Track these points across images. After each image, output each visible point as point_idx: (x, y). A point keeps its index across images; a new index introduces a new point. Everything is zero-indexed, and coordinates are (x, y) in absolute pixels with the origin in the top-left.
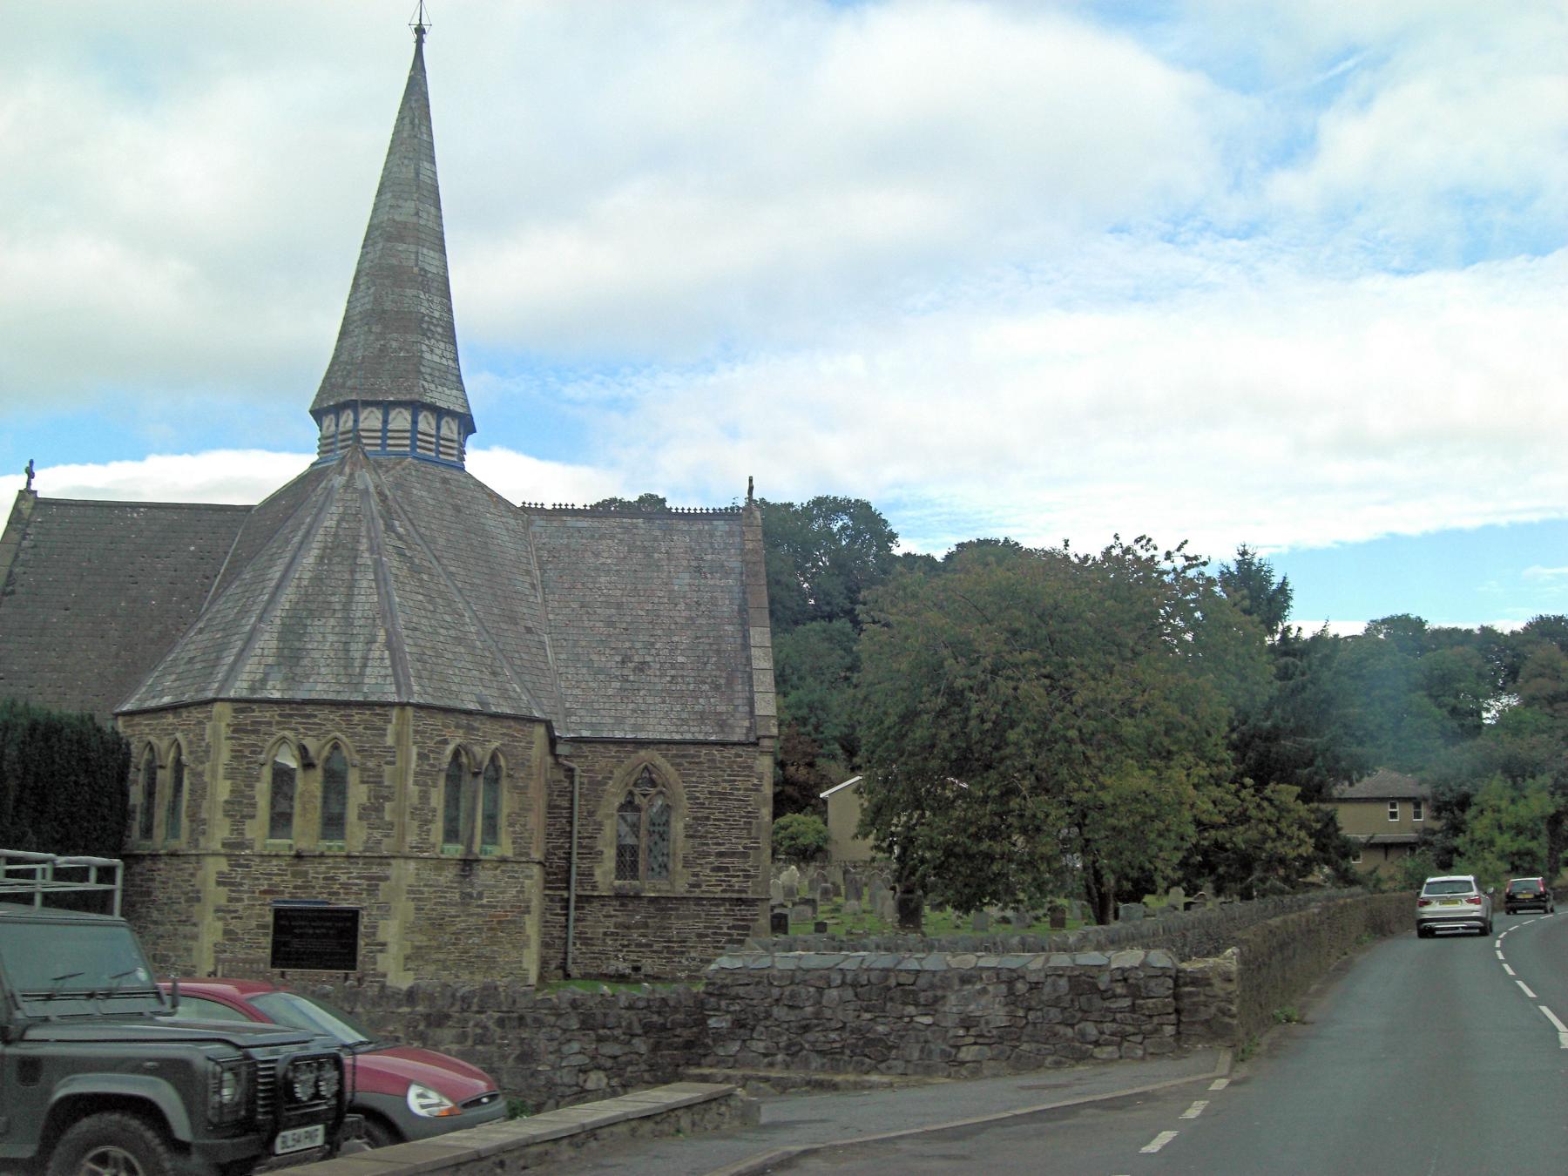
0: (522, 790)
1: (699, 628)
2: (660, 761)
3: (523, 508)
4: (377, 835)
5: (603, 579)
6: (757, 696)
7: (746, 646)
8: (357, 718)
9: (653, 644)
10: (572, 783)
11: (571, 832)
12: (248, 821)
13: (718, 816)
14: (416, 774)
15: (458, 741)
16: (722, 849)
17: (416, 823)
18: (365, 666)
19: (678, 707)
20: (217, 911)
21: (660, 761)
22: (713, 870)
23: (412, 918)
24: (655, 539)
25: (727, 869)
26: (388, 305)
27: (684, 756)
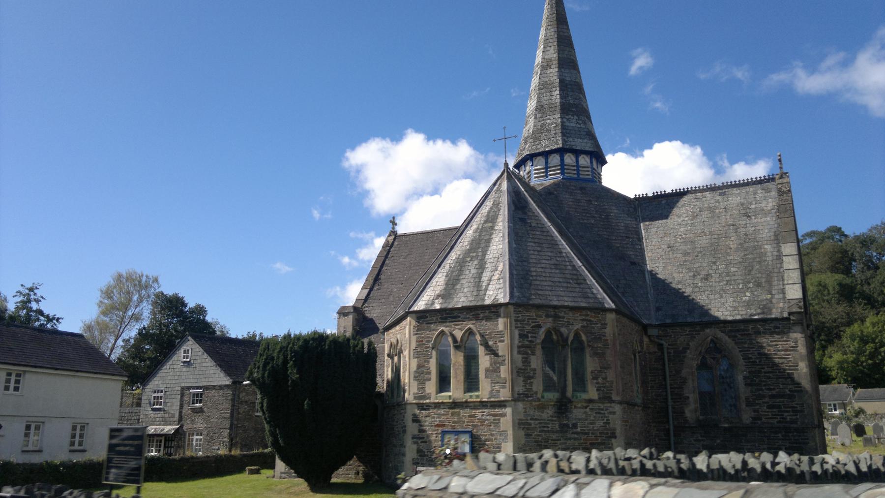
0: (601, 355)
1: (746, 250)
2: (720, 335)
3: (636, 199)
4: (497, 387)
5: (682, 230)
6: (787, 287)
7: (780, 257)
8: (481, 315)
9: (714, 263)
10: (663, 353)
11: (666, 385)
12: (427, 383)
13: (766, 369)
14: (519, 347)
15: (549, 325)
16: (774, 392)
17: (522, 379)
18: (489, 284)
19: (731, 300)
20: (413, 438)
21: (720, 335)
22: (768, 407)
23: (523, 442)
24: (717, 201)
25: (779, 407)
26: (544, 102)
27: (738, 331)
